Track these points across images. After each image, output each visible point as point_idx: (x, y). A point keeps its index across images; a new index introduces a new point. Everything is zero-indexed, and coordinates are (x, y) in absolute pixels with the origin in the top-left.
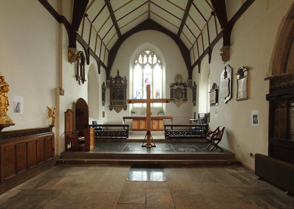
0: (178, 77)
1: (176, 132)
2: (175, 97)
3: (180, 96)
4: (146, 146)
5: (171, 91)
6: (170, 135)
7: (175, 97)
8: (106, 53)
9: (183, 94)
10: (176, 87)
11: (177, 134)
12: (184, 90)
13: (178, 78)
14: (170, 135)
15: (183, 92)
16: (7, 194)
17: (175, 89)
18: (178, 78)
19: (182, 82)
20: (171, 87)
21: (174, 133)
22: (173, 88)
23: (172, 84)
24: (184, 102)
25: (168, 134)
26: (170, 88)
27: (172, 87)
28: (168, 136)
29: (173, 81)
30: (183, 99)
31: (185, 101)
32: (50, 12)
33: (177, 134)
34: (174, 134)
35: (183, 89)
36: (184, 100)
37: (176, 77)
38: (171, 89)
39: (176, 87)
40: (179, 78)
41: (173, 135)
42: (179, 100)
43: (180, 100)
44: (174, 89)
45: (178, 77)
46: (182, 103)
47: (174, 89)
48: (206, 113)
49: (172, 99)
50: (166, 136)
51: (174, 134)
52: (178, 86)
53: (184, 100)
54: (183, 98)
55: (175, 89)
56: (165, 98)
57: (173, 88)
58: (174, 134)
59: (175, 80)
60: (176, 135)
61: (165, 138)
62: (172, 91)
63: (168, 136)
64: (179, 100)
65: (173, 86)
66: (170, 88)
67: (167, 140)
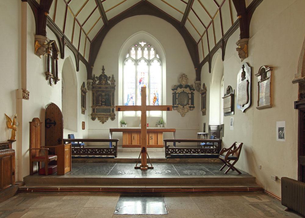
2: (179, 104)
3: (185, 103)
5: (173, 96)
6: (172, 153)
10: (179, 90)
12: (190, 95)
13: (183, 79)
17: (178, 93)
19: (187, 83)
25: (169, 152)
27: (175, 91)
30: (190, 106)
34: (178, 152)
37: (180, 78)
39: (179, 90)
40: (183, 78)
41: (176, 153)
42: (183, 107)
43: (185, 107)
44: (177, 92)
47: (177, 92)
49: (175, 105)
50: (167, 154)
52: (183, 89)
53: (190, 107)
54: (189, 104)
58: (178, 152)
59: (179, 81)
60: (180, 153)
61: (166, 157)
63: (169, 154)
64: (183, 107)
65: (176, 89)
66: (172, 92)
67: (168, 159)
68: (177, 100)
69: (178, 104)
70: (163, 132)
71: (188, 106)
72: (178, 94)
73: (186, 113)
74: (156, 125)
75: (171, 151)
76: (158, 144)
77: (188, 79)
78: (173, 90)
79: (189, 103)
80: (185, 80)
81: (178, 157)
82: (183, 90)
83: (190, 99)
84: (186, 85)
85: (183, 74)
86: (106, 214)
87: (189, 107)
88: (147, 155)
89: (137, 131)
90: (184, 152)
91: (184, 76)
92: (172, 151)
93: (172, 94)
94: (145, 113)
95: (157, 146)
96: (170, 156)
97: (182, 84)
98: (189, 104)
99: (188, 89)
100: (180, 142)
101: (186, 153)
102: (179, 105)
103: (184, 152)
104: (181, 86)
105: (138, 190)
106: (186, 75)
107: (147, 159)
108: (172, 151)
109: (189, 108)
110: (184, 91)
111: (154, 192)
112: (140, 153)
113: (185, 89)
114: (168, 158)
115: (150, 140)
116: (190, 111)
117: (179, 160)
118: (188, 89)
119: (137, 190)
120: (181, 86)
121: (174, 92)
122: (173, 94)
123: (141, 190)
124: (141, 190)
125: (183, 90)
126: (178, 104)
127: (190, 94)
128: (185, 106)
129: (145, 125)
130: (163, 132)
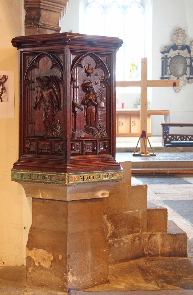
0: (178, 33)
1: (183, 136)
2: (171, 73)
3: (180, 72)
4: (94, 284)
5: (163, 62)
6: (171, 140)
7: (171, 73)
8: (46, 9)
9: (187, 66)
10: (172, 53)
11: (185, 138)
12: (189, 60)
13: (178, 36)
14: (172, 140)
15: (186, 63)
16: (47, 156)
17: (170, 57)
18: (178, 36)
19: (185, 42)
20: (163, 53)
21: (178, 137)
22: (166, 56)
23: (166, 47)
24: (188, 82)
25: (168, 140)
26: (161, 54)
27: (166, 54)
28: (169, 142)
29: (167, 42)
30: (188, 76)
31: (190, 80)
32: (112, 37)
33: (185, 138)
34: (180, 140)
35: (187, 57)
36: (188, 79)
37: (175, 34)
38: (162, 58)
39: (172, 53)
40: (180, 35)
41: (177, 140)
42: (178, 79)
43: (180, 78)
44: (168, 57)
45: (178, 33)
46: (185, 85)
47: (168, 57)
48: (144, 57)
49: (166, 76)
50: (165, 142)
51: (179, 139)
52: (177, 51)
53: (188, 79)
54: (186, 74)
55: (172, 57)
56: (116, 147)
57: (166, 56)
58: (180, 140)
59: (172, 40)
60: (182, 140)
61: (164, 146)
62: (165, 60)
63: (169, 142)
64: (178, 79)
65: (168, 52)
66: (161, 56)
67: (168, 148)
68: (168, 68)
69: (170, 75)
70: (151, 116)
71: (185, 76)
72: (170, 59)
73: (182, 86)
74: (135, 105)
75: (171, 138)
76: (130, 132)
77: (186, 36)
78: (162, 53)
79: (186, 73)
80: (182, 38)
81: (181, 145)
82: (179, 53)
83: (189, 66)
84: (183, 46)
85: (180, 29)
86: (8, 274)
87: (186, 78)
88: (147, 140)
89: (136, 115)
90: (188, 139)
91: (181, 32)
92: (172, 138)
93: (161, 59)
94: (145, 89)
95: (129, 135)
96: (171, 144)
97: (177, 44)
98: (186, 74)
99: (186, 51)
100: (182, 127)
101: (190, 140)
102: (172, 76)
103: (188, 139)
104: (175, 47)
105: (152, 172)
106: (184, 30)
107: (149, 148)
108: (172, 138)
109: (187, 80)
110: (180, 55)
111: (169, 174)
112: (139, 138)
113: (181, 51)
114: (168, 146)
115: (132, 126)
116: (187, 85)
117: (182, 149)
118: (186, 51)
119: (151, 172)
120: (175, 47)
121: (164, 57)
122: (163, 60)
123: (155, 172)
124: (155, 172)
125: (179, 53)
126: (170, 75)
127: (188, 58)
128: (181, 76)
129: (146, 104)
130: (151, 116)
